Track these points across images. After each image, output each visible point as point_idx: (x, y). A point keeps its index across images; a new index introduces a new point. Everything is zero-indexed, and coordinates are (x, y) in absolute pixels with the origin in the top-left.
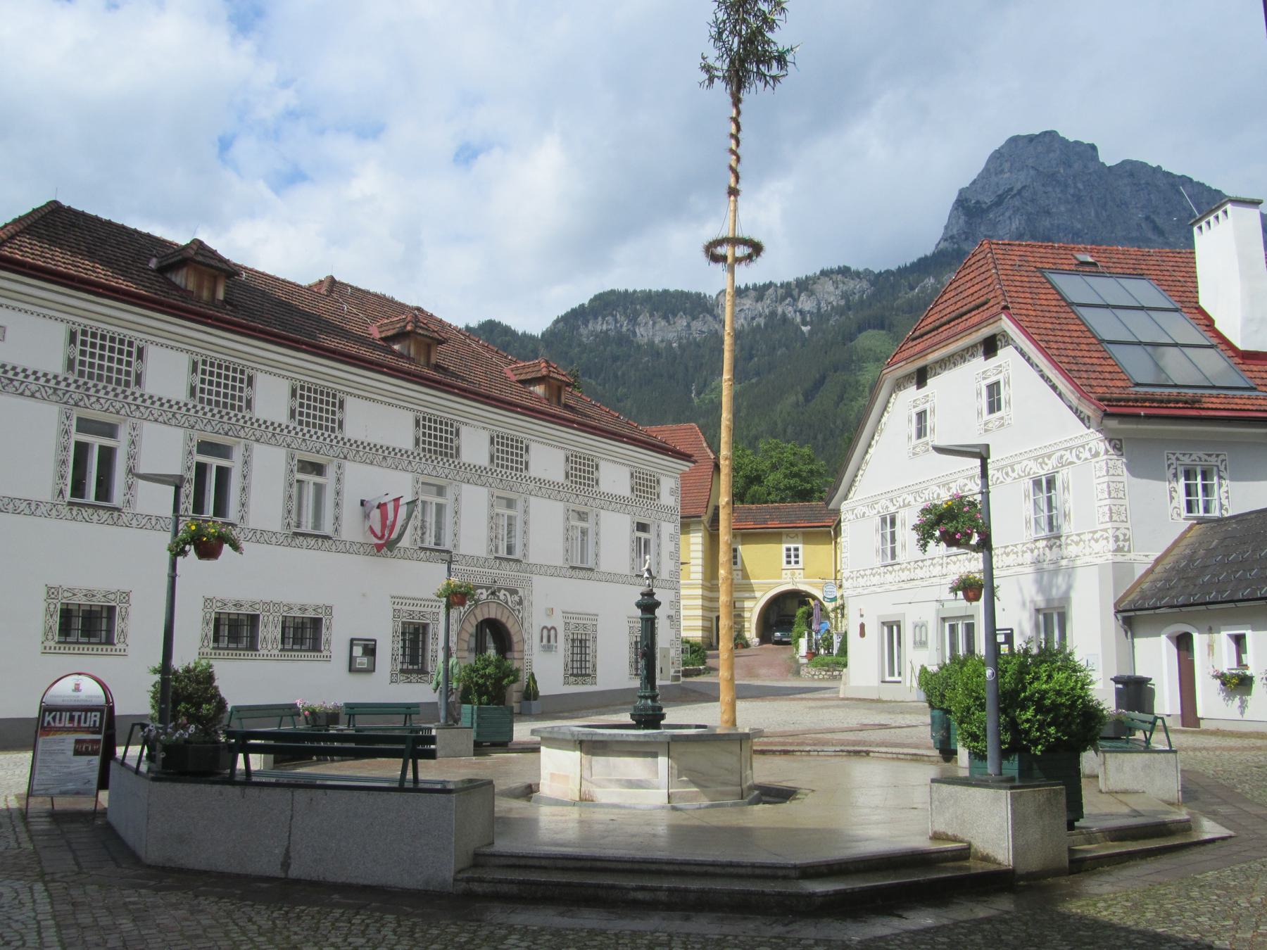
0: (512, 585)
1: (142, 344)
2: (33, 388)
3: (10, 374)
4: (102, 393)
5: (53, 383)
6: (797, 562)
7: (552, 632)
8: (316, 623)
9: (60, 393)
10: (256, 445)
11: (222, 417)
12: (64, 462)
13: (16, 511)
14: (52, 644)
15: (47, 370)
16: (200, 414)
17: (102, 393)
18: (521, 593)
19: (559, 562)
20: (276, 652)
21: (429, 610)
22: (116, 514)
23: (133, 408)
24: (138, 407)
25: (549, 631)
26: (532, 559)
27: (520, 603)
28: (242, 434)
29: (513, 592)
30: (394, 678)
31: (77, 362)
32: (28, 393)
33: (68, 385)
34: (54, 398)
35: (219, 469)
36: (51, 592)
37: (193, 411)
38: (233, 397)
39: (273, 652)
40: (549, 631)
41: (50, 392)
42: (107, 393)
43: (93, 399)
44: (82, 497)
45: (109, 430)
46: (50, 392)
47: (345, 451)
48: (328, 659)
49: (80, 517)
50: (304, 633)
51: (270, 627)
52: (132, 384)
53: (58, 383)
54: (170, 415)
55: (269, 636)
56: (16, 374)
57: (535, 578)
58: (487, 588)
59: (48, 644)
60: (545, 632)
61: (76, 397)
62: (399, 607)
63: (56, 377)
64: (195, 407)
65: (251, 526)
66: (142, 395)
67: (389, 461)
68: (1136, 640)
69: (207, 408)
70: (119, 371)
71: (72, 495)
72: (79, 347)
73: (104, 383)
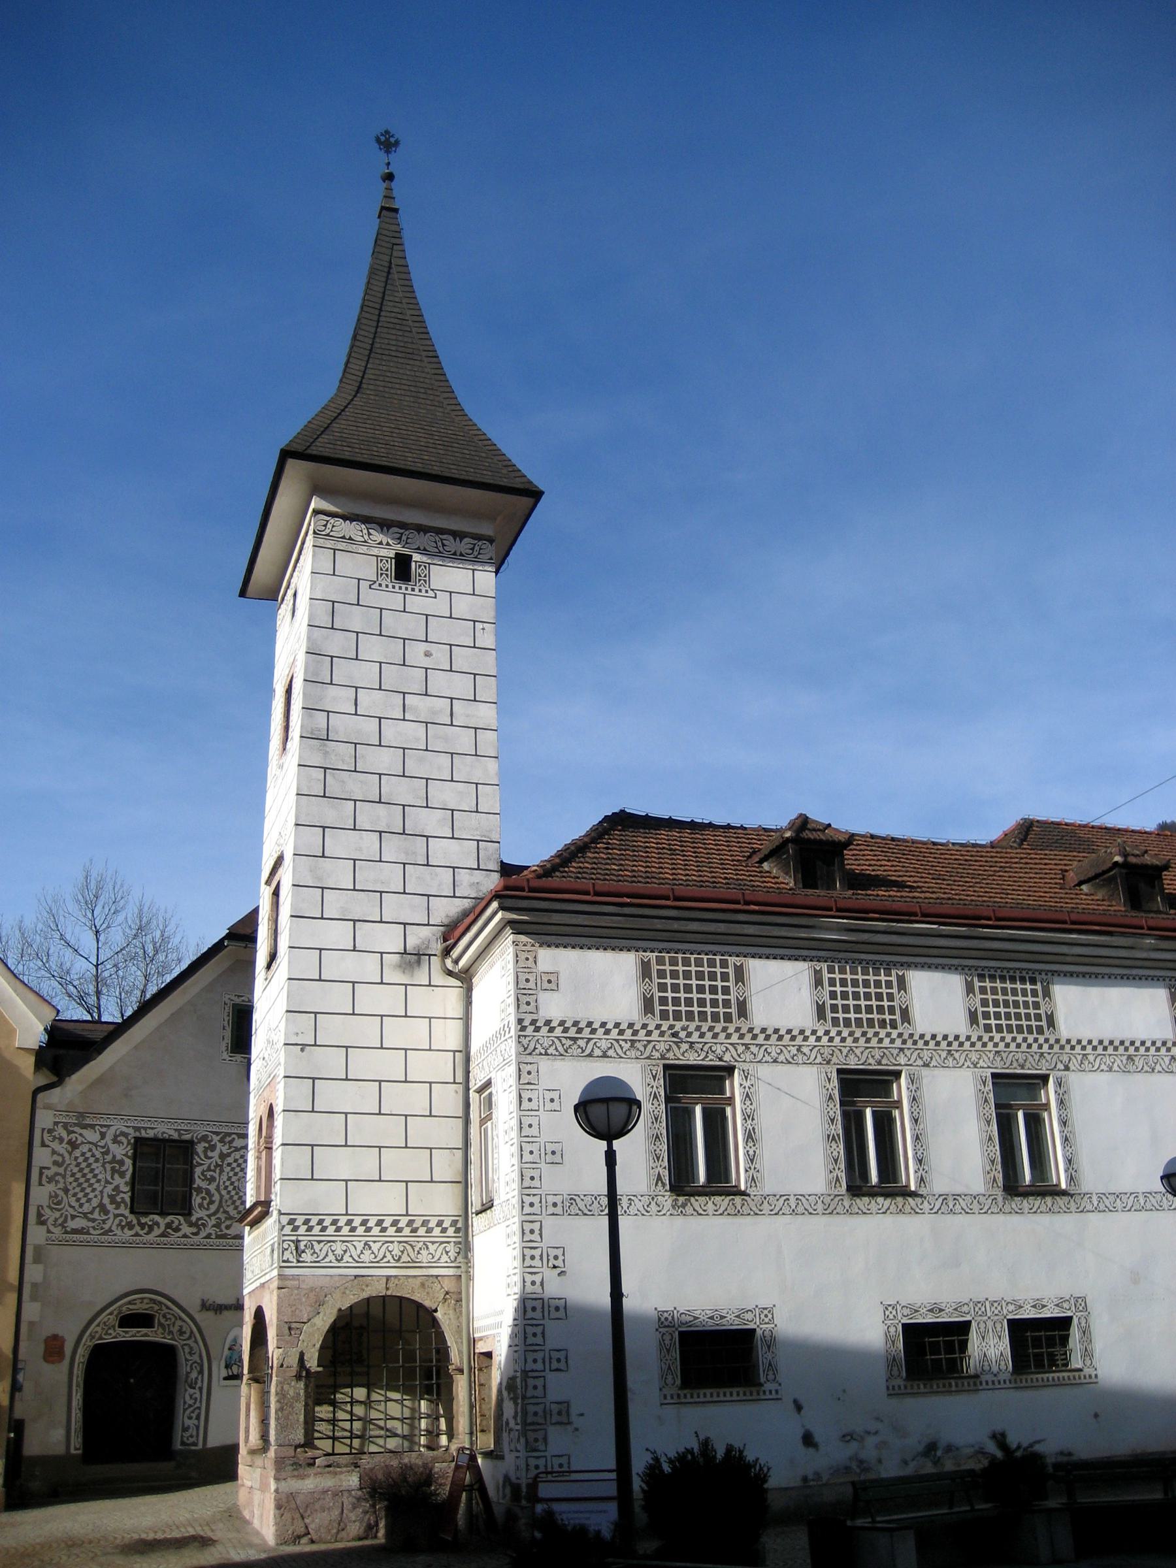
2: (604, 1045)
3: (572, 1032)
9: (639, 1045)
10: (925, 1072)
11: (868, 1041)
12: (1066, 1140)
14: (674, 1391)
15: (1143, 1037)
17: (695, 1037)
22: (738, 1199)
23: (741, 1049)
24: (747, 1046)
32: (597, 1052)
33: (649, 1033)
34: (633, 1053)
37: (825, 1039)
41: (627, 1046)
46: (627, 1046)
52: (735, 1016)
53: (635, 1033)
54: (794, 1050)
56: (580, 1031)
64: (827, 1033)
67: (1139, 1062)
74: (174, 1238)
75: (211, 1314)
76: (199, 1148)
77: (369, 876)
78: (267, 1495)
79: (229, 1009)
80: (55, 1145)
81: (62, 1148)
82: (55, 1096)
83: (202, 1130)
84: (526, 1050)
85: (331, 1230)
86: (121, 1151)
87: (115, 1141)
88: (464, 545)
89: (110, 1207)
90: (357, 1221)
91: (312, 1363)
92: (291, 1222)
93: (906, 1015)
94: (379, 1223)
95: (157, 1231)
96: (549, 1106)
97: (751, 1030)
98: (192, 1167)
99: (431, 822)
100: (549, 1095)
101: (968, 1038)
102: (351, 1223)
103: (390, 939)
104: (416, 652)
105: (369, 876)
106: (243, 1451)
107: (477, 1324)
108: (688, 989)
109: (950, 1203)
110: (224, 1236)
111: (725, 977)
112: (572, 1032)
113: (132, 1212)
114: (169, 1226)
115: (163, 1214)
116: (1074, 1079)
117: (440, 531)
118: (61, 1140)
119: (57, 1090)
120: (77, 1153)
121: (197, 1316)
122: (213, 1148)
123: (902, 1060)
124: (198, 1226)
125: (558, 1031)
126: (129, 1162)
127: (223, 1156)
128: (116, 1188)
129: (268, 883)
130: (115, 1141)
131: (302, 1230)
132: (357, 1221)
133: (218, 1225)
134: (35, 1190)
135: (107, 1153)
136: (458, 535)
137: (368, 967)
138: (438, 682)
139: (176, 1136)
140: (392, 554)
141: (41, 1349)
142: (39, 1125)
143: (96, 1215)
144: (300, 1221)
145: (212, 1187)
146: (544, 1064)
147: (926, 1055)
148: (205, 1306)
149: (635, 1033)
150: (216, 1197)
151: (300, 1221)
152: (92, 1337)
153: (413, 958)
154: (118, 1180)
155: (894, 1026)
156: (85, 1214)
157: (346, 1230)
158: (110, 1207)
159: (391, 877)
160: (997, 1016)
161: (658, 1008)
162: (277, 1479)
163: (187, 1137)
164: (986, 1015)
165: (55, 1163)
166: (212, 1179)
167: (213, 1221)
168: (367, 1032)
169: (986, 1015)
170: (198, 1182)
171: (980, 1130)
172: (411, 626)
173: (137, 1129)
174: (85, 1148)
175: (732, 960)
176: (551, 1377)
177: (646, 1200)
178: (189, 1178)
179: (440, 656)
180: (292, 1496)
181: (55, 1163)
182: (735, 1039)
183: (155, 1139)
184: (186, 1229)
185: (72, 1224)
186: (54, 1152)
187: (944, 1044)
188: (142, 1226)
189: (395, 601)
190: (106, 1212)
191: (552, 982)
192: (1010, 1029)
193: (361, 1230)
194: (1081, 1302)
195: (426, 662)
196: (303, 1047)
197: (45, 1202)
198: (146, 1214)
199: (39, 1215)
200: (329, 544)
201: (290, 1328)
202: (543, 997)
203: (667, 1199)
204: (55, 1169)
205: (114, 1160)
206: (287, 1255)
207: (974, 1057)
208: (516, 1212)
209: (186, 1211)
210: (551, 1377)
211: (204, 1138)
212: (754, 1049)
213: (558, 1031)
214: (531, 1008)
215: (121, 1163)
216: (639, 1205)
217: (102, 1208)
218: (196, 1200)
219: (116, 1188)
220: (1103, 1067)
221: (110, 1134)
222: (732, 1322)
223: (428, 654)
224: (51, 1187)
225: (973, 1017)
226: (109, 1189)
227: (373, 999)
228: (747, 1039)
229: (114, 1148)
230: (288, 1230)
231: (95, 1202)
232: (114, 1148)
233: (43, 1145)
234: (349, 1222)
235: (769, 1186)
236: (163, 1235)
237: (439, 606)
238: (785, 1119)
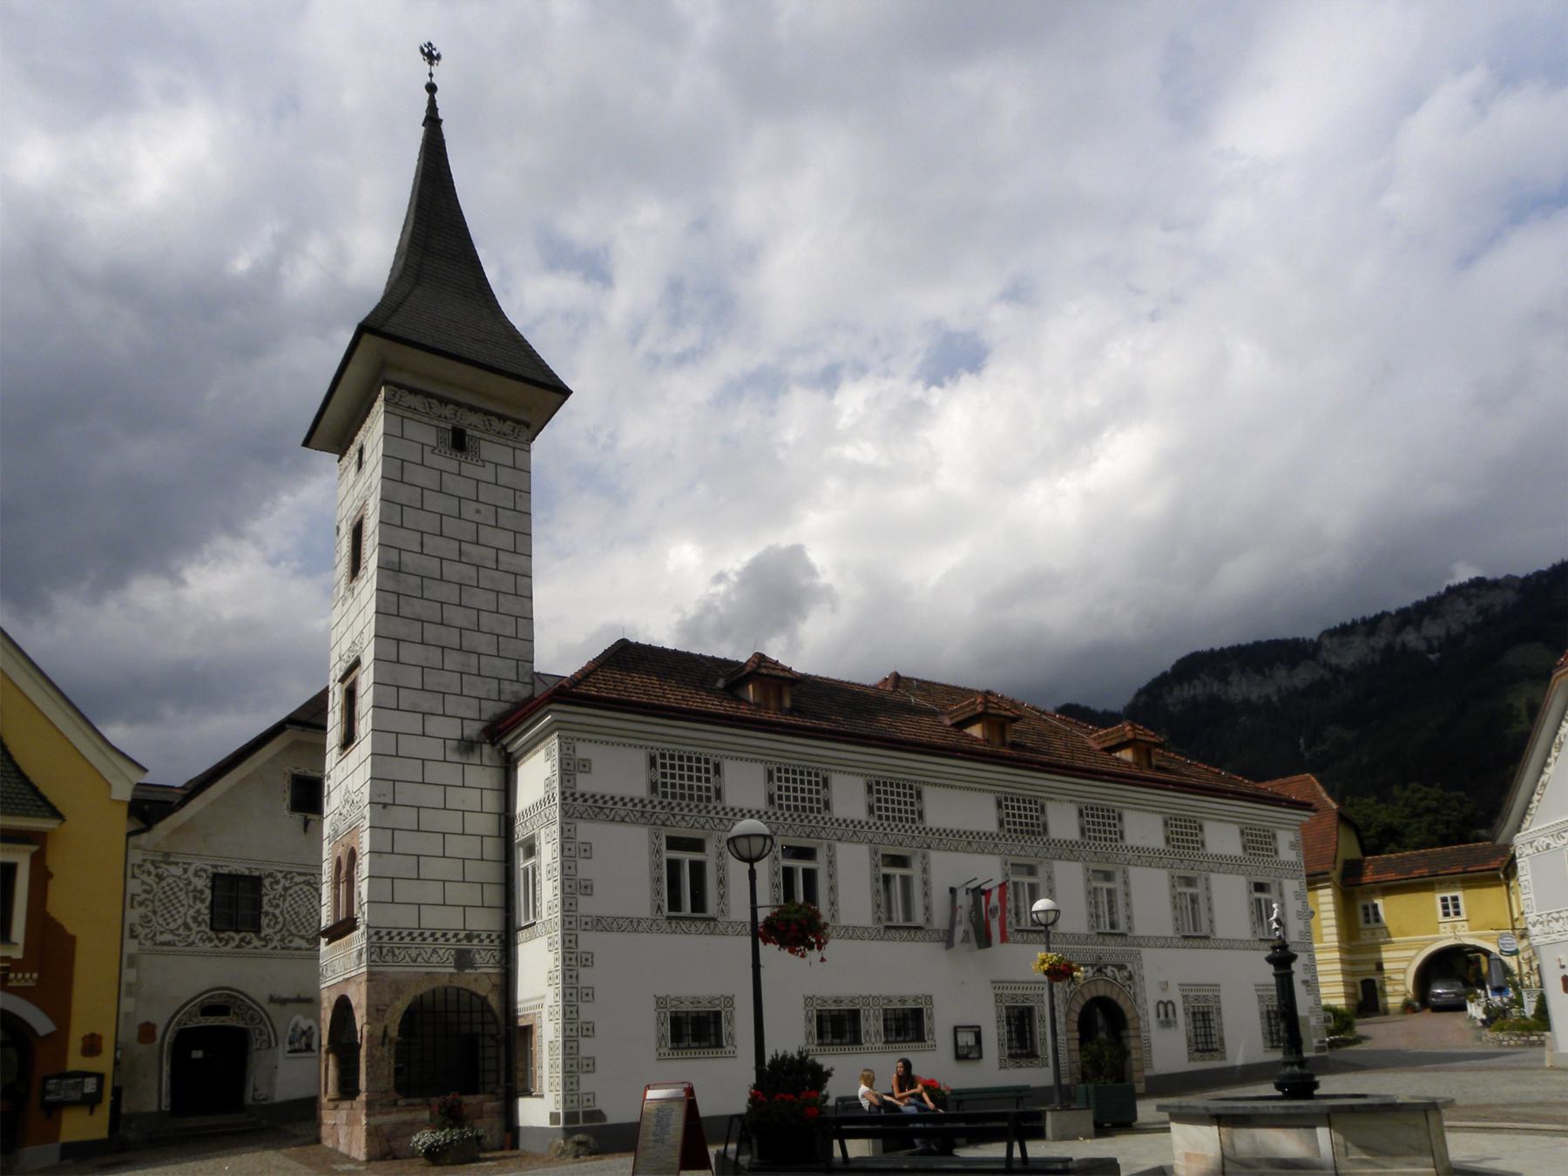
0: (1118, 961)
1: (826, 774)
2: (623, 813)
3: (600, 803)
4: (686, 811)
5: (639, 807)
6: (1457, 914)
10: (838, 845)
13: (620, 929)
14: (666, 1050)
17: (686, 811)
18: (1130, 967)
19: (1168, 930)
25: (1166, 1005)
27: (1130, 977)
28: (823, 835)
29: (1121, 967)
36: (660, 1002)
38: (811, 800)
45: (697, 845)
48: (933, 1048)
51: (872, 1021)
58: (1092, 966)
60: (1161, 1007)
67: (975, 846)
72: (660, 770)
74: (247, 949)
75: (277, 1006)
76: (267, 882)
77: (433, 680)
78: (357, 1128)
79: (288, 778)
80: (144, 877)
81: (151, 880)
82: (144, 839)
83: (269, 869)
84: (565, 813)
85: (407, 939)
86: (201, 883)
87: (196, 874)
88: (507, 427)
89: (193, 926)
90: (427, 934)
91: (394, 1032)
92: (377, 933)
93: (827, 805)
94: (444, 935)
95: (233, 944)
98: (261, 896)
99: (483, 643)
102: (419, 935)
103: (452, 729)
104: (469, 509)
105: (433, 680)
106: (324, 1100)
107: (519, 1006)
108: (795, 790)
109: (1231, 944)
110: (288, 948)
111: (707, 771)
112: (600, 803)
113: (212, 929)
114: (242, 940)
115: (237, 931)
117: (487, 413)
118: (149, 873)
119: (145, 836)
120: (164, 883)
121: (267, 1008)
122: (277, 882)
124: (267, 940)
125: (590, 802)
126: (208, 893)
127: (286, 889)
128: (198, 911)
129: (342, 680)
130: (196, 874)
131: (386, 939)
132: (427, 934)
133: (282, 940)
134: (129, 912)
135: (189, 883)
136: (503, 418)
137: (434, 749)
138: (487, 534)
139: (247, 873)
140: (449, 427)
141: (136, 1032)
142: (130, 861)
143: (181, 931)
145: (277, 912)
148: (272, 1000)
150: (281, 919)
151: (383, 933)
152: (178, 1023)
153: (467, 746)
154: (198, 905)
155: (819, 811)
156: (172, 931)
157: (419, 940)
158: (193, 926)
159: (452, 681)
160: (887, 809)
161: (660, 789)
162: (367, 1115)
163: (256, 874)
164: (879, 809)
165: (145, 891)
166: (277, 906)
167: (278, 937)
168: (432, 796)
169: (879, 809)
170: (266, 908)
172: (465, 488)
173: (215, 867)
174: (171, 880)
176: (582, 1041)
178: (258, 904)
179: (487, 514)
180: (377, 1128)
181: (145, 891)
182: (713, 814)
183: (230, 875)
184: (256, 943)
185: (160, 938)
186: (143, 883)
188: (220, 940)
189: (451, 465)
190: (189, 929)
191: (585, 766)
192: (901, 819)
193: (430, 940)
194: (929, 999)
195: (478, 518)
196: (385, 806)
197: (137, 920)
198: (223, 931)
199: (132, 931)
200: (398, 411)
201: (375, 1011)
202: (579, 777)
204: (144, 896)
205: (195, 890)
206: (374, 957)
207: (870, 836)
208: (559, 927)
209: (256, 928)
210: (582, 1041)
211: (270, 875)
213: (590, 802)
215: (202, 892)
217: (187, 926)
218: (264, 921)
219: (198, 911)
221: (191, 870)
222: (705, 1007)
223: (478, 511)
224: (142, 910)
225: (871, 810)
226: (192, 912)
227: (436, 772)
228: (721, 815)
229: (195, 881)
230: (374, 939)
231: (180, 922)
232: (195, 881)
233: (134, 876)
234: (421, 934)
236: (238, 946)
237: (487, 474)
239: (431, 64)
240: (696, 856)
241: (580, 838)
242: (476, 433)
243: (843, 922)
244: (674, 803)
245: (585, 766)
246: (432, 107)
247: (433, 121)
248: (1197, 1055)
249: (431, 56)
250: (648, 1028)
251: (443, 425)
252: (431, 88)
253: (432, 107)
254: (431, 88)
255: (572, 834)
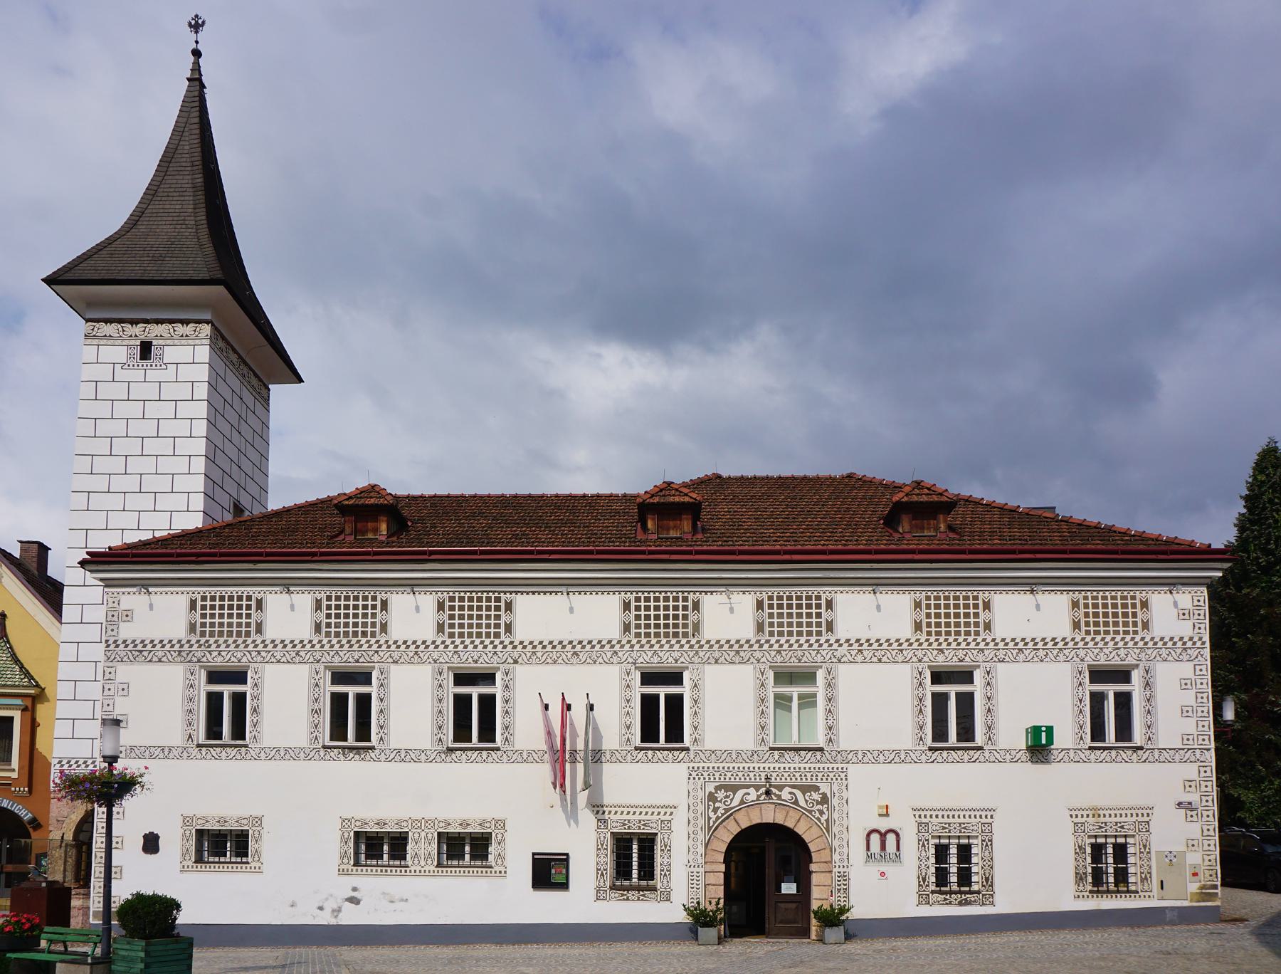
0: (808, 780)
2: (160, 654)
3: (140, 647)
4: (223, 647)
5: (177, 647)
7: (891, 838)
8: (648, 843)
9: (184, 654)
10: (393, 667)
11: (351, 646)
14: (190, 863)
15: (609, 637)
16: (327, 647)
17: (223, 647)
20: (432, 868)
21: (973, 820)
22: (243, 749)
23: (254, 654)
24: (259, 652)
25: (883, 836)
26: (844, 743)
27: (824, 800)
30: (601, 894)
31: (198, 625)
32: (155, 659)
33: (191, 646)
34: (179, 659)
35: (1118, 695)
39: (427, 868)
40: (883, 836)
41: (175, 654)
42: (228, 646)
43: (215, 654)
44: (947, 741)
46: (175, 654)
47: (516, 655)
49: (209, 756)
50: (466, 847)
51: (423, 844)
53: (182, 646)
54: (293, 654)
55: (422, 853)
56: (145, 646)
57: (852, 769)
58: (757, 788)
59: (185, 863)
60: (875, 838)
61: (199, 654)
62: (1079, 820)
63: (748, 641)
64: (320, 642)
65: (392, 747)
66: (1152, 639)
67: (583, 656)
68: (606, 802)
69: (477, 641)
70: (239, 625)
71: (934, 740)
73: (795, 638)
96: (121, 693)
97: (994, 640)
100: (121, 686)
101: (434, 642)
108: (356, 616)
109: (404, 755)
112: (140, 647)
116: (843, 670)
123: (819, 658)
140: (138, 343)
144: (73, 762)
146: (121, 668)
147: (1164, 652)
149: (182, 646)
171: (433, 706)
172: (150, 391)
175: (691, 596)
177: (180, 750)
187: (412, 648)
189: (139, 374)
191: (128, 616)
203: (1025, 756)
212: (263, 654)
214: (115, 633)
216: (176, 753)
220: (549, 660)
235: (844, 743)
237: (169, 374)
238: (287, 700)
239: (197, 32)
240: (363, 689)
241: (119, 679)
242: (161, 342)
243: (708, 745)
244: (212, 640)
245: (128, 616)
246: (196, 68)
247: (196, 81)
248: (658, 882)
249: (196, 26)
250: (333, 846)
251: (133, 342)
252: (197, 53)
253: (196, 68)
254: (197, 53)
255: (112, 676)
